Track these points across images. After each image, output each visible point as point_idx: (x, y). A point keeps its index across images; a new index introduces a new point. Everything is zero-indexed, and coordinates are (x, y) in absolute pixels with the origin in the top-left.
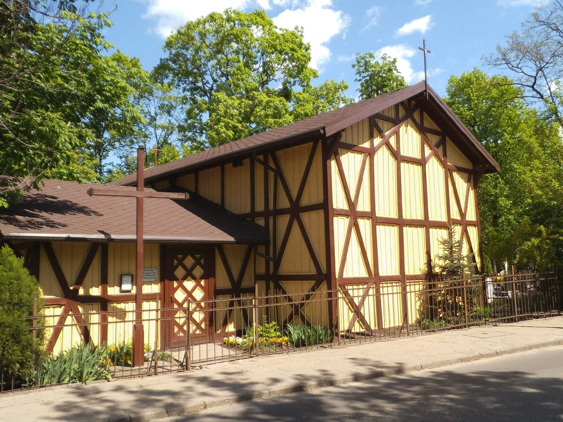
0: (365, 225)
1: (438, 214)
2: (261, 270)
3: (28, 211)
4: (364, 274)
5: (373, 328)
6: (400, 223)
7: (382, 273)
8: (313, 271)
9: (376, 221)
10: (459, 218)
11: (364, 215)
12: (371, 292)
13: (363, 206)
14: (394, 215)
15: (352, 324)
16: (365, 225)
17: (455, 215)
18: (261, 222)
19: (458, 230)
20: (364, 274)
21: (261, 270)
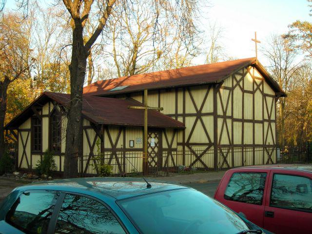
0: (229, 121)
1: (259, 117)
2: (181, 141)
3: (136, 107)
4: (267, 98)
5: (230, 166)
6: (243, 121)
7: (235, 143)
8: (207, 142)
9: (234, 120)
10: (268, 119)
11: (229, 117)
12: (231, 151)
13: (229, 113)
14: (240, 117)
15: (223, 164)
16: (229, 121)
17: (266, 117)
18: (180, 119)
19: (266, 124)
20: (267, 98)
21: (181, 141)
